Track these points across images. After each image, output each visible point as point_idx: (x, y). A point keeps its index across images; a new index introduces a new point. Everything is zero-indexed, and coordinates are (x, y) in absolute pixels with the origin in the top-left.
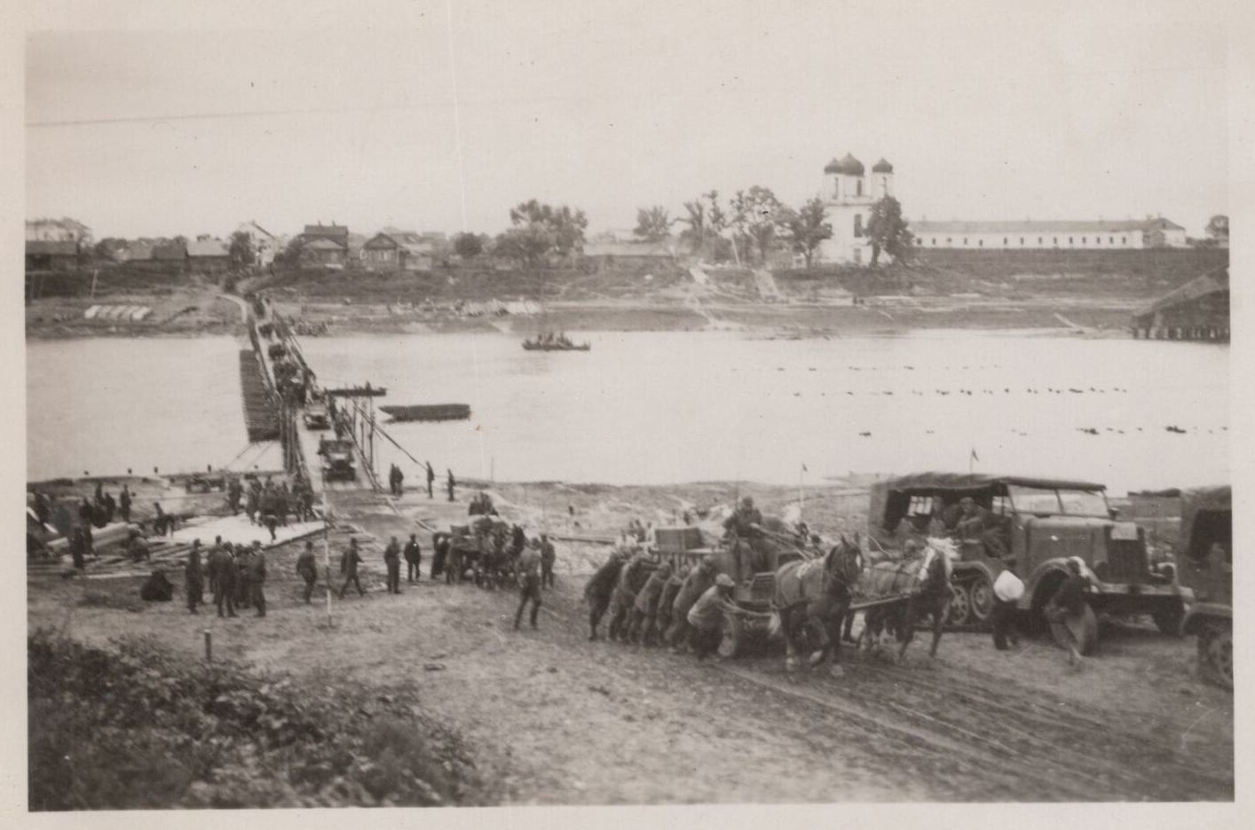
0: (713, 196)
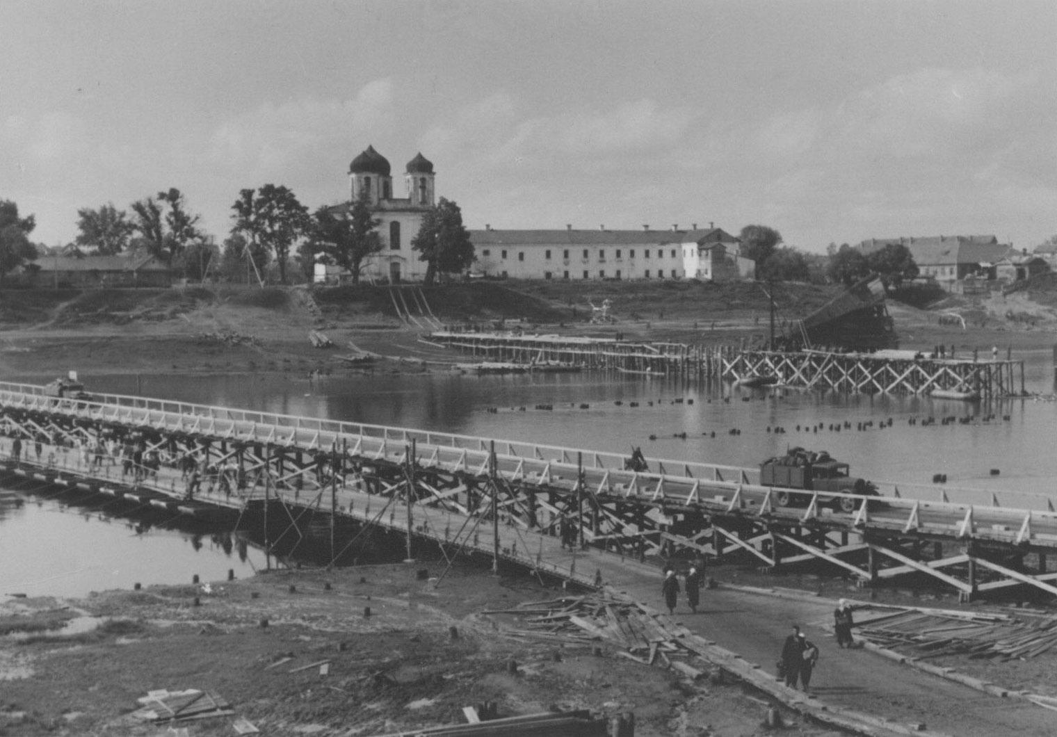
0: (173, 196)
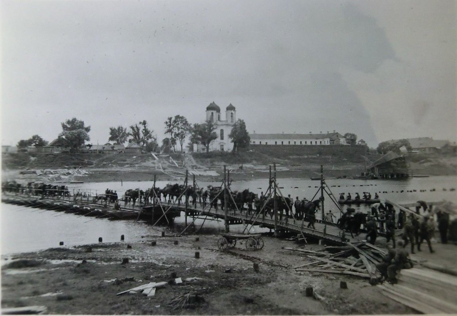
0: (144, 123)
